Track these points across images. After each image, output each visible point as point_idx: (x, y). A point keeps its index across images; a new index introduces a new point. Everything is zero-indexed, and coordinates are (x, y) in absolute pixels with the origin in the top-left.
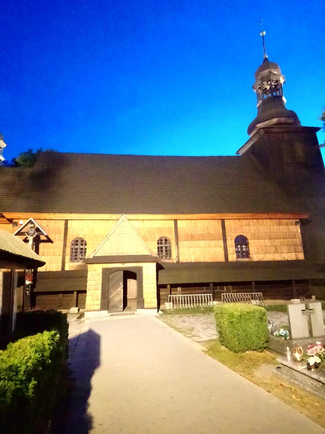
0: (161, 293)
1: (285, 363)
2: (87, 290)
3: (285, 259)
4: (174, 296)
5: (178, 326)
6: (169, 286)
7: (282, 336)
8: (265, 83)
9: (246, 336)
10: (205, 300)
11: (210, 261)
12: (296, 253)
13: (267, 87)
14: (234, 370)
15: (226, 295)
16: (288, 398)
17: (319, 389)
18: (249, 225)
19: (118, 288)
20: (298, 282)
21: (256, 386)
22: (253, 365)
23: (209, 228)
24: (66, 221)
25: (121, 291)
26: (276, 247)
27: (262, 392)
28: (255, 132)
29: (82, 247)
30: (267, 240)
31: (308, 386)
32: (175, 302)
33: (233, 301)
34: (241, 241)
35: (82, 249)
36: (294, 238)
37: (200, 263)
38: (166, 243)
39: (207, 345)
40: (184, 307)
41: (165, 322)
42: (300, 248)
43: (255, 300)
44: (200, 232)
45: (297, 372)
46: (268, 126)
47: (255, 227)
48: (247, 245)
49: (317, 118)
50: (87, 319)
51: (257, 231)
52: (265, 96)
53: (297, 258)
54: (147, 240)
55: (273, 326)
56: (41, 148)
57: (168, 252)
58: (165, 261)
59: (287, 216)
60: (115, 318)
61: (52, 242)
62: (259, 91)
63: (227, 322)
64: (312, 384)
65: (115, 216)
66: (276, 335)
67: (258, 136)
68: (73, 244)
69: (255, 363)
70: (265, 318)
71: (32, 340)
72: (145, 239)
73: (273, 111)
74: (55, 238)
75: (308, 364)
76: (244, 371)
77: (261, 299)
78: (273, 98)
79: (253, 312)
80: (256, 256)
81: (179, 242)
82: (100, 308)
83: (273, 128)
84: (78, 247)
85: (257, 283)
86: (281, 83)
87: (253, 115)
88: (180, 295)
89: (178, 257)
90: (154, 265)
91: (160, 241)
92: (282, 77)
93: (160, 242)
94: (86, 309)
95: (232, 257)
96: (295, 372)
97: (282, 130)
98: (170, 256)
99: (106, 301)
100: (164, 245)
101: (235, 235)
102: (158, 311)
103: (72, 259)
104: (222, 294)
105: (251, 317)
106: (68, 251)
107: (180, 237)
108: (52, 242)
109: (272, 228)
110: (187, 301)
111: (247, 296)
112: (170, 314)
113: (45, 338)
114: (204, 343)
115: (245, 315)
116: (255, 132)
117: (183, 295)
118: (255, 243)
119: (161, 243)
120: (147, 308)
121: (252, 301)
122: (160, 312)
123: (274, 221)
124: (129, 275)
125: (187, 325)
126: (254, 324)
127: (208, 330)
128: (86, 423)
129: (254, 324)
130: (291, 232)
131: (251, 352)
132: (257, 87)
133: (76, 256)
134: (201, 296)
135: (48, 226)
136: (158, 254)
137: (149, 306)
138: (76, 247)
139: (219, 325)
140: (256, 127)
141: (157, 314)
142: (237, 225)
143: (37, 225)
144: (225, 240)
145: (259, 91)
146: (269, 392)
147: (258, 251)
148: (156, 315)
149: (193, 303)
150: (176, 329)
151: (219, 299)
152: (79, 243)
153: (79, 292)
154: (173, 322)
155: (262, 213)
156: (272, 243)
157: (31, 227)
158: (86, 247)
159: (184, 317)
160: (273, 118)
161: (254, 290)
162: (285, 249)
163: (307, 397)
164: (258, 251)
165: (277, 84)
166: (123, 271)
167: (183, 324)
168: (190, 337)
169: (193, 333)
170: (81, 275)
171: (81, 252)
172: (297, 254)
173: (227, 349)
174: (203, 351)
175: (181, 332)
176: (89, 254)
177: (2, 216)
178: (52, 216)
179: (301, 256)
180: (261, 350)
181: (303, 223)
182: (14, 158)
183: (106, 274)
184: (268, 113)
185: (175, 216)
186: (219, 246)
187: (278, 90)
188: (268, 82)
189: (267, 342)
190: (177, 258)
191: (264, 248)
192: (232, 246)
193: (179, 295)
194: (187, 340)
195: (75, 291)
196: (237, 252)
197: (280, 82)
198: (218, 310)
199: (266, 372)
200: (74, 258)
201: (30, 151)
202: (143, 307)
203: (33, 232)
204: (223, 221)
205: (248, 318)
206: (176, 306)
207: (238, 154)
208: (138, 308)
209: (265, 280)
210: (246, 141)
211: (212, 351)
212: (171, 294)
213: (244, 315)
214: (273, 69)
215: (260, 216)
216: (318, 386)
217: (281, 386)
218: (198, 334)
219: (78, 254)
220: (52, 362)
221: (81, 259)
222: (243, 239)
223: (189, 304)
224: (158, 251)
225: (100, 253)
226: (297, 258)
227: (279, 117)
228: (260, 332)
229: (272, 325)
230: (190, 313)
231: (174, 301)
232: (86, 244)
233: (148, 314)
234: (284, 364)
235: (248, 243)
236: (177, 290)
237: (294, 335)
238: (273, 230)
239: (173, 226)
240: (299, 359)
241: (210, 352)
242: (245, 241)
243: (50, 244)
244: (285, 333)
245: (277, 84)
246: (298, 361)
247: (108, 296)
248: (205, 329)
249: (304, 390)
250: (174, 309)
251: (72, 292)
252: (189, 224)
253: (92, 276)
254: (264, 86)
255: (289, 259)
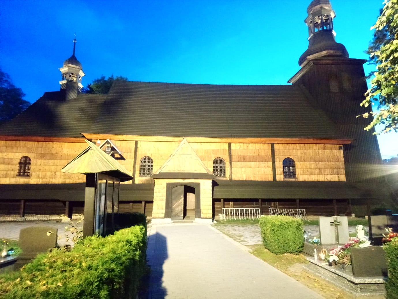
0: (216, 206)
1: (312, 261)
2: (154, 200)
3: (328, 180)
4: (227, 209)
5: (230, 233)
6: (222, 200)
7: (315, 243)
8: (316, 17)
9: (285, 241)
10: (254, 214)
11: (259, 180)
12: (338, 175)
13: (318, 21)
14: (273, 266)
15: (273, 210)
16: (311, 285)
17: (335, 279)
18: (297, 149)
19: (180, 200)
20: (339, 201)
21: (288, 276)
22: (288, 263)
23: (260, 150)
24: (136, 142)
25: (181, 202)
26: (320, 169)
27: (293, 280)
28: (305, 63)
29: (149, 164)
30: (312, 163)
31: (328, 277)
32: (227, 214)
33: (278, 214)
34: (289, 163)
35: (149, 166)
36: (337, 162)
37: (251, 181)
38: (221, 163)
39: (253, 248)
40: (235, 218)
41: (218, 230)
42: (343, 171)
43: (298, 215)
44: (251, 155)
45: (321, 268)
46: (318, 58)
47: (302, 151)
48: (294, 166)
49: (363, 52)
50: (153, 224)
51: (303, 155)
52: (316, 30)
53: (339, 179)
54: (204, 160)
55: (308, 235)
56: (112, 76)
57: (222, 171)
58: (219, 178)
59: (332, 142)
60: (177, 224)
61: (124, 159)
62: (311, 25)
63: (270, 230)
64: (330, 276)
65: (177, 139)
66: (310, 242)
67: (308, 68)
68: (141, 162)
69: (291, 262)
70: (301, 227)
71: (129, 230)
72: (203, 159)
73: (323, 44)
74: (127, 156)
75: (328, 261)
76: (280, 267)
77: (304, 214)
78: (323, 33)
79: (291, 223)
80: (302, 176)
81: (232, 162)
82: (164, 216)
83: (322, 60)
84: (147, 164)
85: (301, 200)
86: (331, 18)
87: (304, 47)
88: (232, 209)
89: (231, 175)
90: (210, 182)
91: (215, 162)
92: (333, 12)
93: (215, 162)
94: (153, 217)
95: (280, 177)
96: (319, 268)
97: (331, 62)
98: (224, 175)
99: (170, 210)
100: (219, 165)
101: (283, 158)
102: (213, 221)
103: (141, 174)
104: (269, 209)
105: (289, 227)
106: (138, 167)
107: (234, 156)
108: (124, 159)
109: (317, 152)
110: (238, 213)
111: (290, 211)
112: (223, 223)
113: (137, 229)
114: (251, 247)
115: (285, 224)
116: (305, 63)
117: (234, 209)
118: (301, 165)
119: (217, 163)
120: (204, 218)
121: (296, 216)
122: (215, 222)
123: (320, 145)
124: (189, 189)
125: (237, 233)
126: (291, 232)
127: (255, 237)
128: (163, 293)
129: (291, 232)
130: (335, 156)
131: (289, 254)
132: (309, 21)
133: (144, 171)
134: (251, 210)
135: (121, 145)
136: (214, 172)
137: (205, 216)
138: (144, 164)
139: (263, 233)
140: (307, 59)
141: (212, 223)
142: (285, 149)
143: (112, 145)
144: (274, 162)
145: (311, 25)
146: (297, 280)
147: (304, 172)
148: (211, 224)
149: (244, 215)
150: (227, 235)
151: (267, 214)
152: (147, 161)
153: (146, 202)
154: (226, 230)
155: (308, 138)
156: (316, 166)
157: (108, 147)
158: (152, 164)
159: (235, 226)
160: (321, 51)
161: (298, 206)
162: (328, 171)
163: (326, 285)
164: (304, 172)
165: (328, 18)
166: (183, 186)
167: (234, 232)
168: (239, 242)
169: (242, 239)
170: (149, 188)
171: (149, 169)
172: (339, 176)
173: (269, 252)
174: (250, 252)
175: (232, 238)
176: (155, 171)
177: (82, 137)
178: (124, 137)
179: (343, 178)
180: (296, 253)
181: (347, 148)
182: (90, 84)
183: (170, 188)
184: (317, 46)
185: (229, 140)
186: (268, 166)
187: (329, 24)
188: (319, 17)
189: (302, 247)
190: (230, 176)
191: (309, 170)
192: (280, 168)
193: (231, 208)
194: (237, 244)
195: (144, 201)
196: (285, 173)
197: (331, 17)
198: (263, 220)
199: (297, 268)
200: (142, 174)
201: (103, 78)
202: (200, 217)
203: (109, 151)
204: (272, 145)
205: (287, 227)
206: (229, 218)
207: (290, 83)
208: (196, 217)
209: (309, 197)
210: (297, 72)
211: (257, 252)
212: (224, 207)
213: (283, 224)
214: (324, 5)
215: (307, 141)
216: (335, 277)
217: (308, 278)
218: (246, 240)
219: (146, 170)
220: (143, 244)
221: (148, 174)
222: (290, 161)
223: (240, 216)
224: (214, 170)
225: (165, 170)
226: (339, 179)
227: (328, 50)
228: (297, 239)
229: (307, 234)
230: (240, 223)
231: (227, 214)
232: (152, 162)
233: (205, 222)
234: (311, 262)
235: (295, 165)
236: (229, 204)
237: (323, 242)
238: (318, 154)
239: (227, 148)
240: (323, 258)
241: (255, 253)
242: (293, 163)
243: (123, 161)
244: (317, 241)
245: (327, 18)
246: (322, 260)
247: (171, 207)
248: (252, 236)
249: (324, 280)
250: (226, 220)
251: (140, 202)
252: (241, 147)
253: (158, 189)
254: (315, 20)
255: (332, 180)
